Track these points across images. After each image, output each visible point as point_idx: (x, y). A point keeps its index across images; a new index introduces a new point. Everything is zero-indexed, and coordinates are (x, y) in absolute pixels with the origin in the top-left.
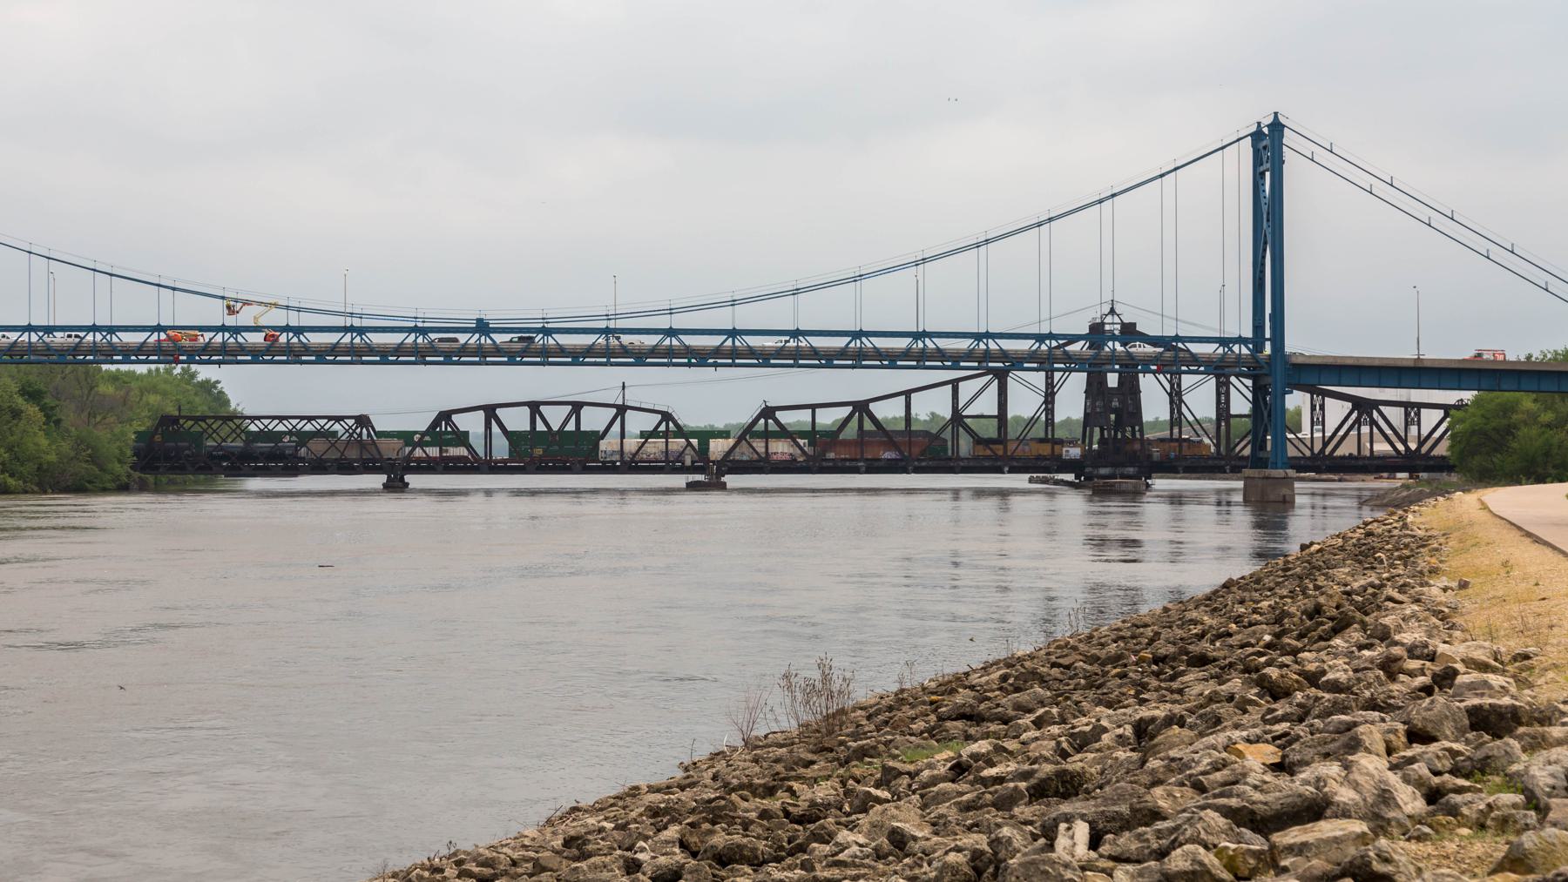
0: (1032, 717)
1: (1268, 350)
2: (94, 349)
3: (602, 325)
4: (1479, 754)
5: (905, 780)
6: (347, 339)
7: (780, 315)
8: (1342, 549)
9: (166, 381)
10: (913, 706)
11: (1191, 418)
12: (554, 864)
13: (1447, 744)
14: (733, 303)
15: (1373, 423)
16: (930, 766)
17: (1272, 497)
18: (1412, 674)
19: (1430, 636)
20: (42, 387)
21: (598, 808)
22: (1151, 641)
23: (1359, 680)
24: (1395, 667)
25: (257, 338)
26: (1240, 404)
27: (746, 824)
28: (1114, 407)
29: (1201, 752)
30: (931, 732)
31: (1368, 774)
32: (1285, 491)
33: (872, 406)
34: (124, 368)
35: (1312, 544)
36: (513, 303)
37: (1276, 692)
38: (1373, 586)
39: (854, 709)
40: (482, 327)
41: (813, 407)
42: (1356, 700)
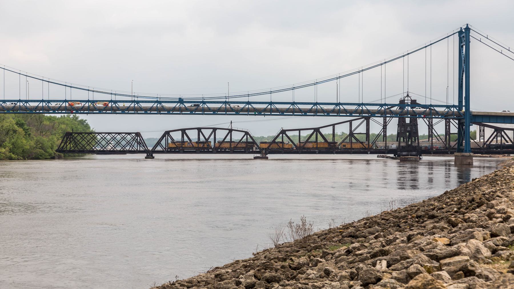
0: (374, 236)
1: (464, 109)
2: (43, 108)
3: (224, 100)
4: (511, 240)
5: (330, 256)
6: (133, 105)
7: (287, 96)
8: (486, 180)
9: (67, 120)
10: (334, 233)
11: (436, 135)
12: (212, 282)
13: (502, 237)
14: (271, 92)
15: (502, 136)
16: (339, 251)
17: (465, 163)
18: (497, 218)
19: (508, 207)
20: (23, 122)
21: (226, 267)
22: (417, 211)
23: (479, 219)
24: (492, 216)
25: (100, 105)
26: (454, 129)
27: (277, 270)
28: (408, 131)
29: (423, 241)
30: (340, 241)
31: (473, 244)
32: (469, 161)
33: (321, 130)
34: (53, 115)
35: (476, 179)
36: (192, 92)
37: (454, 225)
38: (493, 192)
39: (313, 235)
40: (181, 101)
41: (300, 130)
42: (476, 225)
